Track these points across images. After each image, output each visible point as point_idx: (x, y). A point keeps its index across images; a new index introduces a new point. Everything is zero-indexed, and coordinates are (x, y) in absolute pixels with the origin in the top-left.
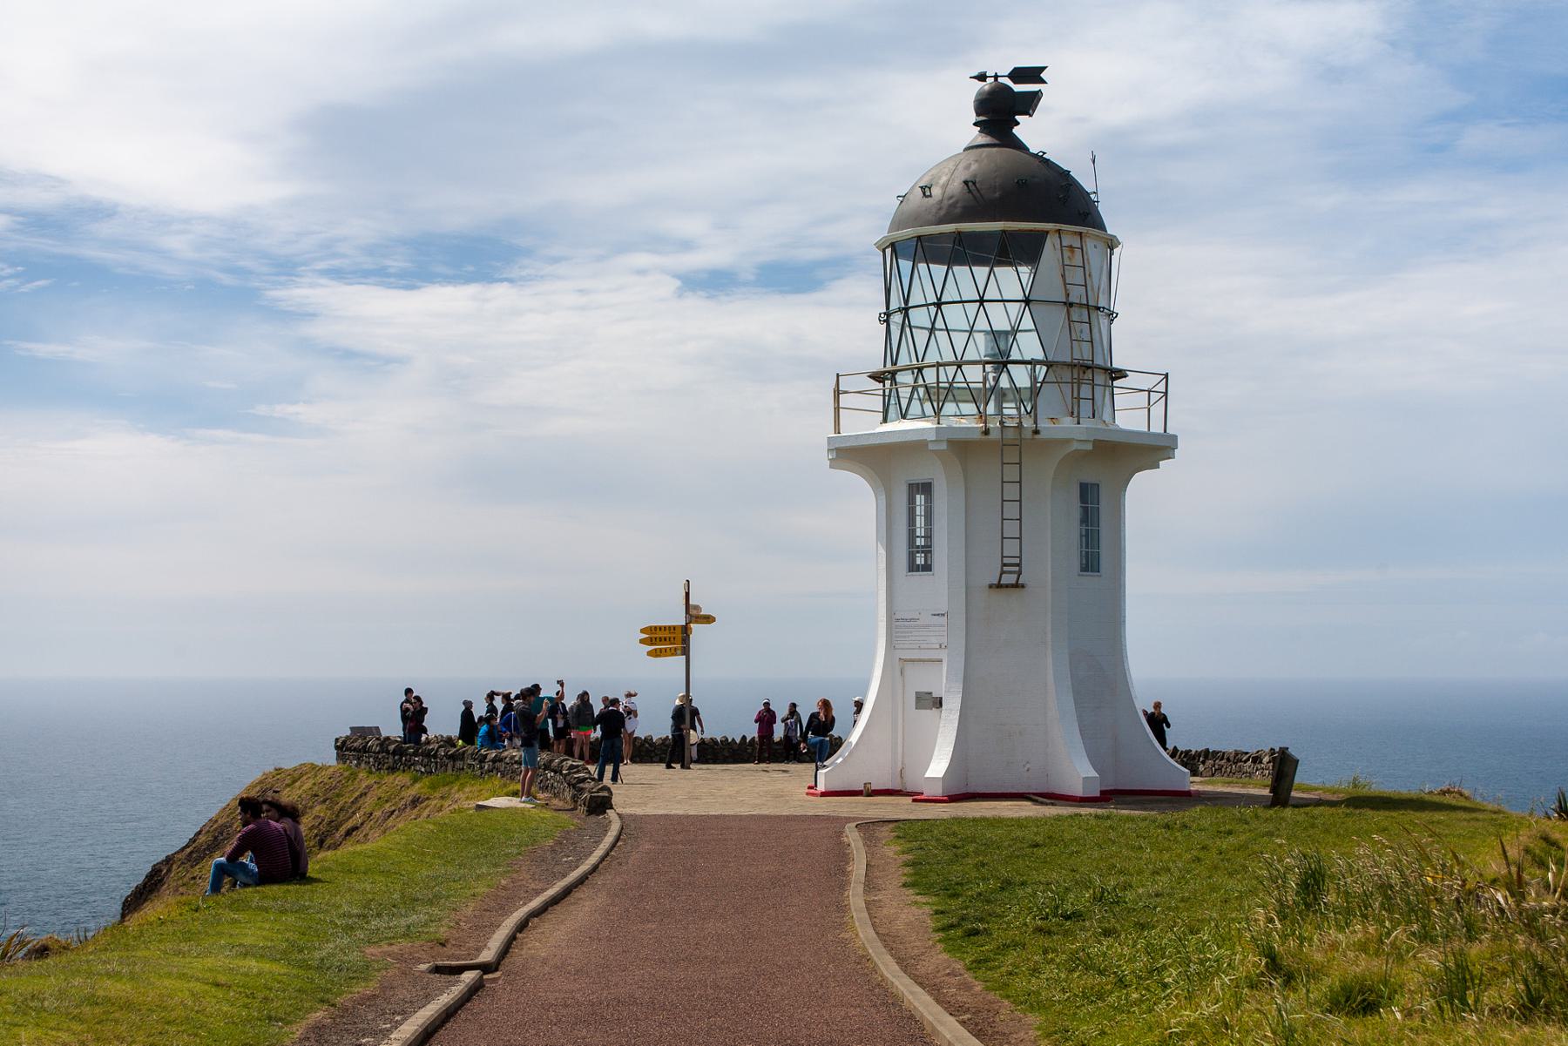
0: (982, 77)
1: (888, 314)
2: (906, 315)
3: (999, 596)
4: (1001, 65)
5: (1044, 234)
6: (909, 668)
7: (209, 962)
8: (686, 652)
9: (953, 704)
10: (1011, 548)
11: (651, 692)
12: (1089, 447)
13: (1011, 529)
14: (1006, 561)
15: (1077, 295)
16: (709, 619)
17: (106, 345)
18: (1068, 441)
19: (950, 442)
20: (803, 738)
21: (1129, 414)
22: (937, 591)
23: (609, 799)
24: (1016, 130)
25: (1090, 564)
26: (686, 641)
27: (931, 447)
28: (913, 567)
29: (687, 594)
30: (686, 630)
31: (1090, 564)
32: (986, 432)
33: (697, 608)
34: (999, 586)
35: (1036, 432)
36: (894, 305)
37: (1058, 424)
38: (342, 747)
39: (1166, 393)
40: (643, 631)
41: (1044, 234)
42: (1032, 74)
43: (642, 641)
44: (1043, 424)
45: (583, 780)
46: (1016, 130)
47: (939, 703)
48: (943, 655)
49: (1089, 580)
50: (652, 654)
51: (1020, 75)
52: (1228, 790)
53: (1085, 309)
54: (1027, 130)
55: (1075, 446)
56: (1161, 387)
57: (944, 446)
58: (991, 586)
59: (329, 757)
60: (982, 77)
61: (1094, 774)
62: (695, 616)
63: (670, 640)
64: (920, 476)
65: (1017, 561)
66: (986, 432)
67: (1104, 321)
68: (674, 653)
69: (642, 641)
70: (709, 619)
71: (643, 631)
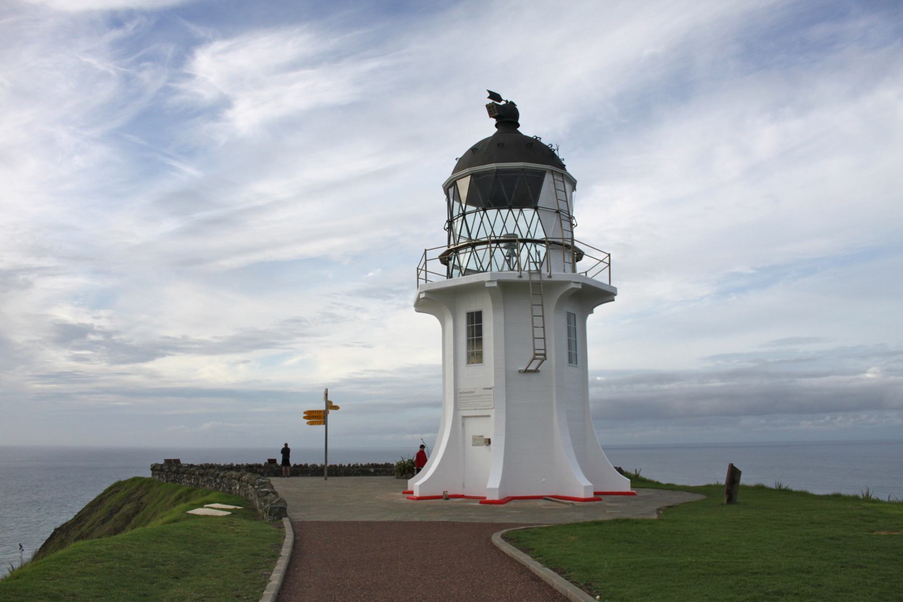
1: (451, 222)
2: (464, 218)
6: (468, 421)
7: (85, 578)
8: (325, 423)
9: (499, 444)
12: (580, 286)
13: (539, 333)
14: (537, 352)
15: (562, 206)
16: (336, 408)
18: (568, 282)
22: (486, 374)
23: (285, 509)
24: (519, 129)
27: (487, 285)
28: (469, 361)
29: (326, 395)
30: (325, 413)
32: (521, 276)
33: (331, 402)
34: (526, 371)
35: (550, 277)
36: (455, 213)
37: (558, 272)
38: (154, 468)
39: (609, 264)
40: (305, 413)
41: (541, 175)
43: (305, 418)
45: (267, 493)
46: (519, 129)
47: (489, 442)
48: (492, 413)
50: (311, 423)
52: (46, 386)
53: (565, 216)
55: (573, 285)
56: (607, 260)
57: (495, 284)
58: (520, 371)
59: (148, 474)
61: (589, 484)
62: (330, 406)
63: (317, 417)
64: (474, 308)
65: (543, 352)
66: (521, 276)
67: (568, 187)
68: (319, 423)
69: (305, 418)
70: (336, 408)
71: (305, 413)
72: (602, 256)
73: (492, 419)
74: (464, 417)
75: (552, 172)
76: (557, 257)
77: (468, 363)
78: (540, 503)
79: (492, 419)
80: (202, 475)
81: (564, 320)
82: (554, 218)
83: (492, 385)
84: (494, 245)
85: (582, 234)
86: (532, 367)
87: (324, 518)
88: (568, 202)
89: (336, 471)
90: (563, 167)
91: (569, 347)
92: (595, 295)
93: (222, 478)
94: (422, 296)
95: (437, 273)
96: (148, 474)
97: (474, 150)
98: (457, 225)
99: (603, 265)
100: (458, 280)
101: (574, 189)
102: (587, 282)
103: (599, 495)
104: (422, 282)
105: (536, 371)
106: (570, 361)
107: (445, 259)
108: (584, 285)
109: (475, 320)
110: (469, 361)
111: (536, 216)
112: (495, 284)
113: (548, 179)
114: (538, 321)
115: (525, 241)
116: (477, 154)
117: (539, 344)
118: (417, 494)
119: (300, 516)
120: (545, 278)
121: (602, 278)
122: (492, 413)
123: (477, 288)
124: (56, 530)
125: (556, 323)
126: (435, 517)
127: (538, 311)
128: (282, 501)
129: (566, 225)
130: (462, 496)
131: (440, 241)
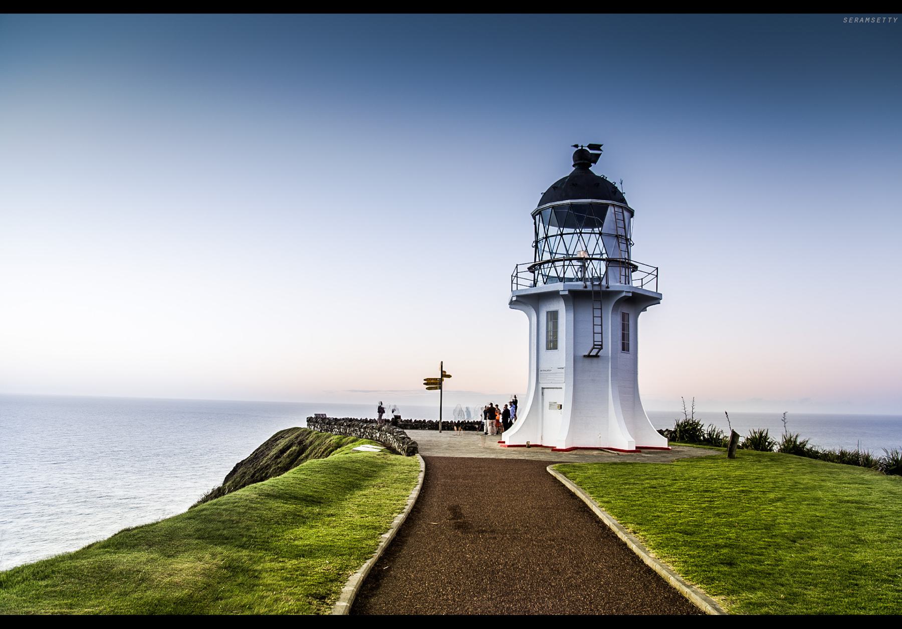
0: (576, 146)
1: (537, 242)
3: (588, 361)
4: (584, 144)
5: (607, 206)
8: (441, 388)
10: (598, 338)
11: (425, 406)
12: (630, 295)
13: (598, 329)
15: (621, 232)
16: (449, 376)
17: (551, 324)
18: (622, 292)
19: (569, 291)
20: (501, 418)
21: (639, 281)
22: (561, 358)
25: (625, 348)
26: (441, 384)
27: (561, 293)
28: (548, 348)
30: (441, 380)
31: (625, 348)
32: (586, 287)
34: (589, 356)
35: (608, 287)
37: (615, 284)
41: (607, 206)
42: (597, 147)
44: (610, 284)
45: (404, 438)
47: (550, 405)
49: (625, 356)
51: (591, 147)
53: (623, 239)
54: (596, 169)
55: (624, 294)
59: (304, 425)
60: (576, 146)
62: (444, 375)
63: (434, 384)
66: (586, 287)
67: (626, 214)
68: (436, 388)
70: (449, 376)
72: (650, 270)
73: (563, 391)
74: (543, 388)
75: (613, 205)
76: (615, 272)
77: (547, 349)
78: (595, 452)
79: (563, 391)
80: (349, 426)
81: (619, 319)
82: (614, 242)
83: (564, 366)
84: (567, 263)
85: (636, 256)
86: (594, 353)
87: (441, 455)
88: (626, 228)
89: (448, 426)
90: (623, 200)
91: (623, 339)
92: (641, 301)
93: (365, 428)
94: (514, 299)
95: (525, 283)
96: (304, 425)
97: (554, 187)
98: (541, 245)
99: (651, 277)
100: (541, 287)
101: (632, 216)
102: (637, 291)
103: (639, 449)
104: (515, 286)
105: (597, 356)
106: (623, 350)
107: (532, 269)
108: (633, 293)
109: (553, 316)
110: (548, 348)
111: (600, 241)
112: (567, 293)
113: (611, 210)
114: (598, 321)
115: (591, 259)
116: (556, 191)
117: (598, 338)
118: (507, 443)
119: (427, 454)
120: (604, 289)
121: (650, 287)
122: (563, 386)
123: (553, 295)
124: (237, 465)
125: (611, 322)
126: (516, 457)
127: (597, 313)
128: (414, 443)
129: (623, 246)
130: (541, 446)
131: (529, 258)
